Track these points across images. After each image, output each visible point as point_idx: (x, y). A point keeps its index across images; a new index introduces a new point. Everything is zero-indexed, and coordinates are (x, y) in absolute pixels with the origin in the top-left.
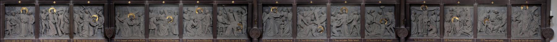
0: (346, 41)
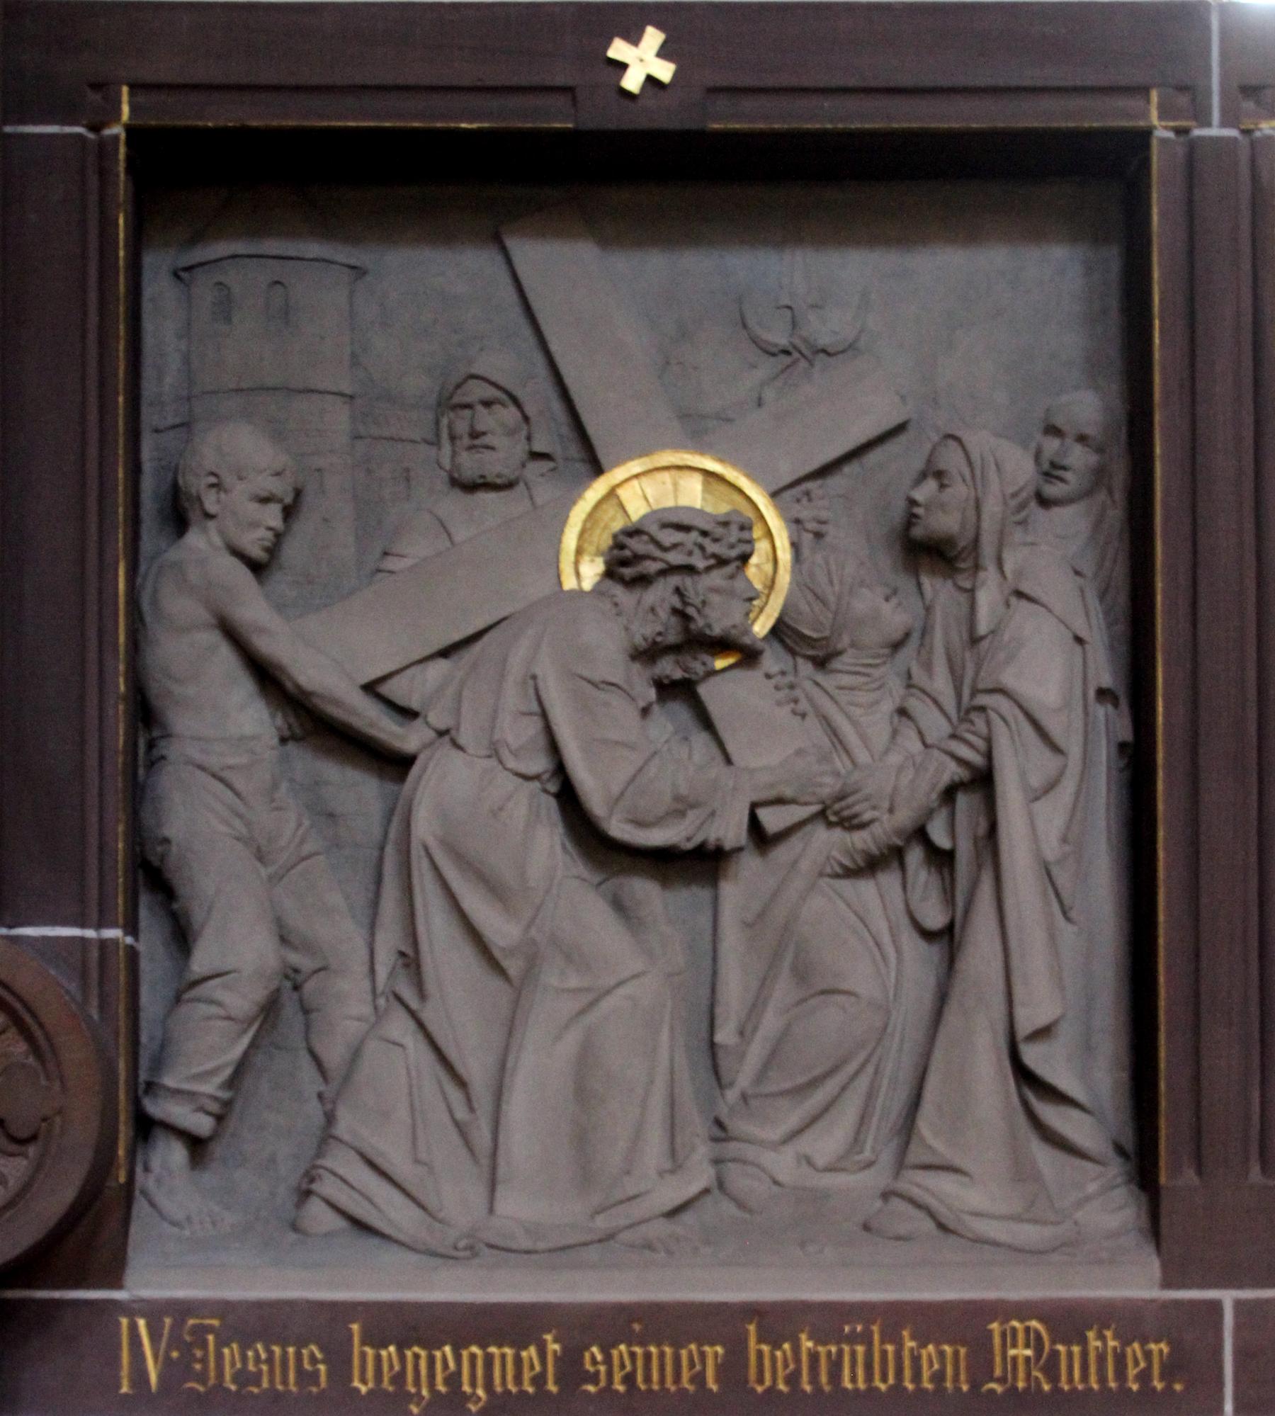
0: (277, 1366)
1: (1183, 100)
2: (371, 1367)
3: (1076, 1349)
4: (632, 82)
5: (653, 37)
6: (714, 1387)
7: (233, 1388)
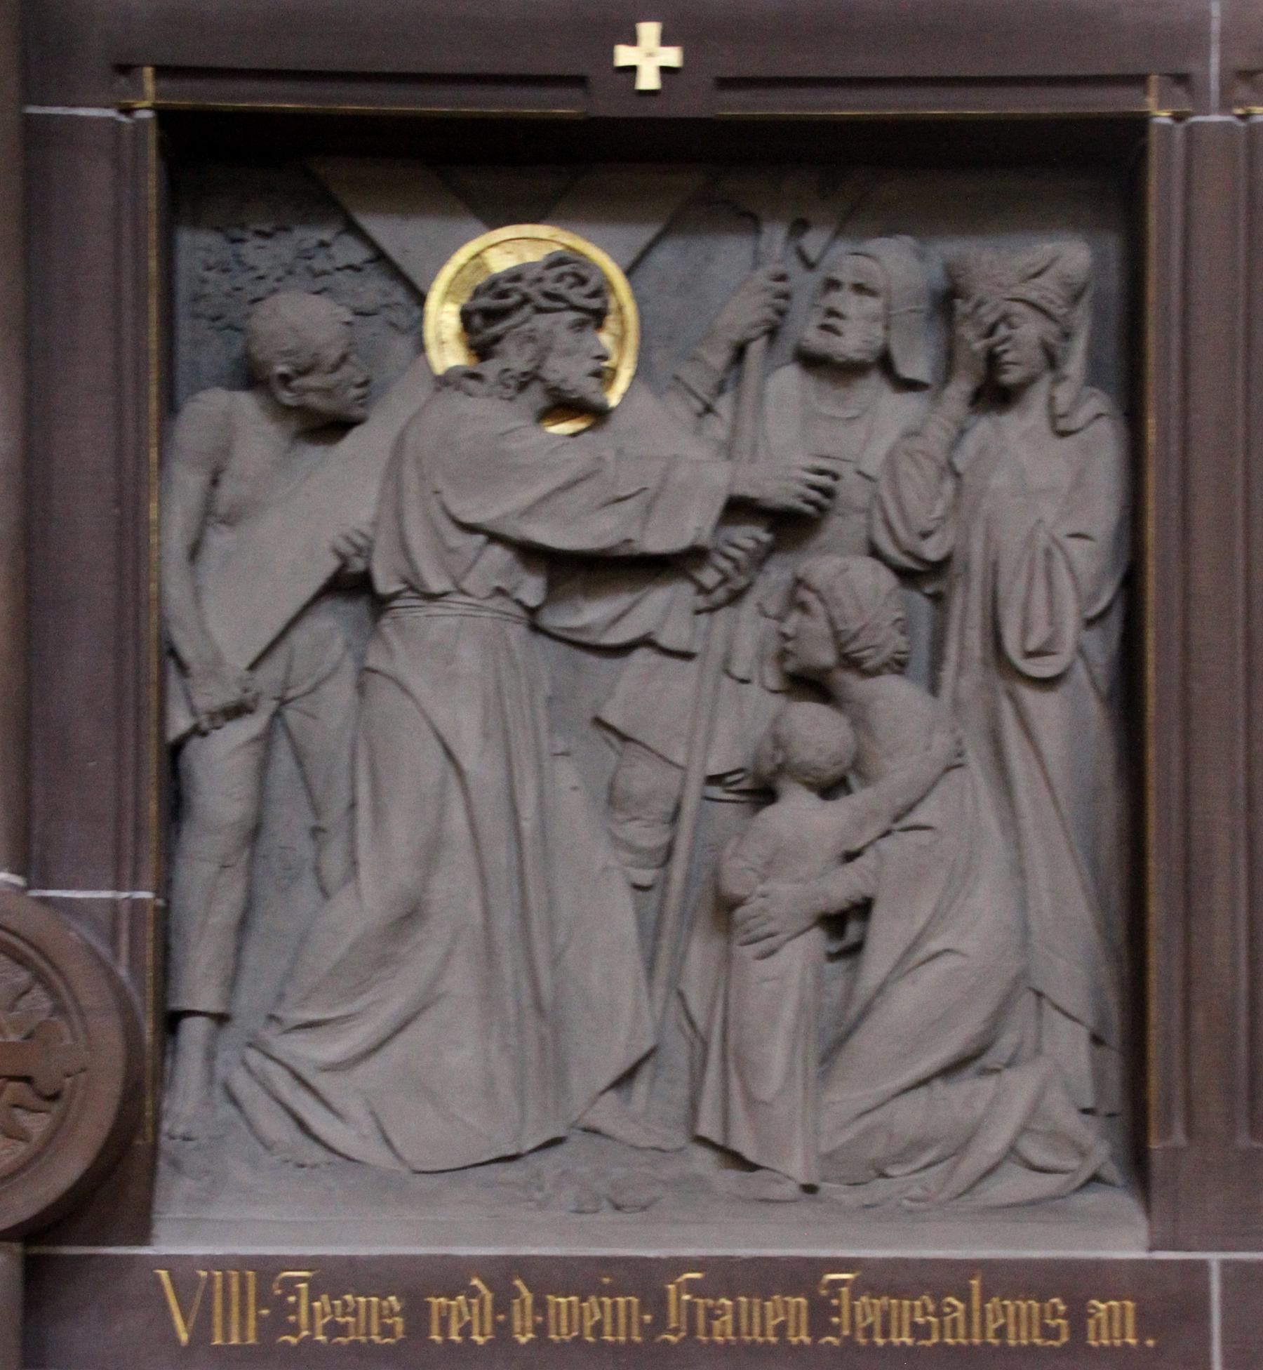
2: (313, 1316)
4: (648, 80)
5: (649, 31)
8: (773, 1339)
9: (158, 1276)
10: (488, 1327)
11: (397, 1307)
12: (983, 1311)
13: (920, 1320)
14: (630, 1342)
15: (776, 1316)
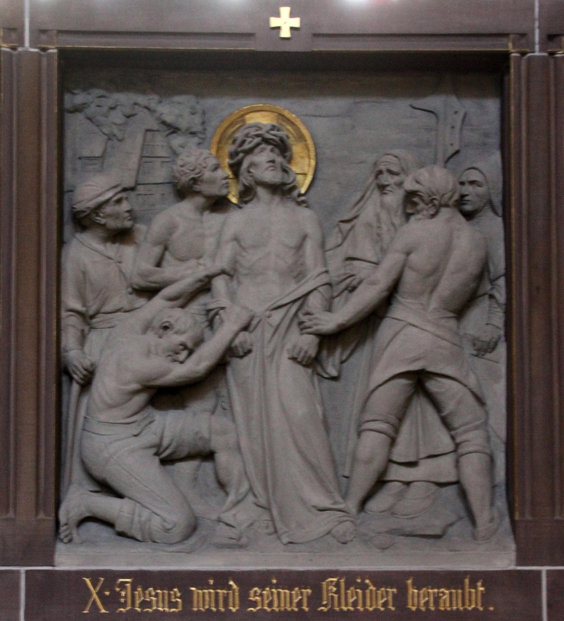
1: (14, 36)
3: (460, 591)
5: (285, 11)
6: (307, 609)
7: (139, 610)
8: (296, 609)
9: (84, 580)
10: (237, 602)
11: (179, 594)
12: (346, 594)
13: (173, 600)
14: (418, 610)
15: (352, 597)
